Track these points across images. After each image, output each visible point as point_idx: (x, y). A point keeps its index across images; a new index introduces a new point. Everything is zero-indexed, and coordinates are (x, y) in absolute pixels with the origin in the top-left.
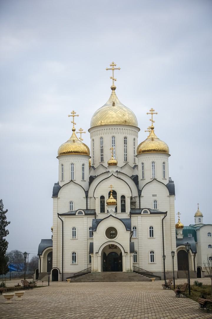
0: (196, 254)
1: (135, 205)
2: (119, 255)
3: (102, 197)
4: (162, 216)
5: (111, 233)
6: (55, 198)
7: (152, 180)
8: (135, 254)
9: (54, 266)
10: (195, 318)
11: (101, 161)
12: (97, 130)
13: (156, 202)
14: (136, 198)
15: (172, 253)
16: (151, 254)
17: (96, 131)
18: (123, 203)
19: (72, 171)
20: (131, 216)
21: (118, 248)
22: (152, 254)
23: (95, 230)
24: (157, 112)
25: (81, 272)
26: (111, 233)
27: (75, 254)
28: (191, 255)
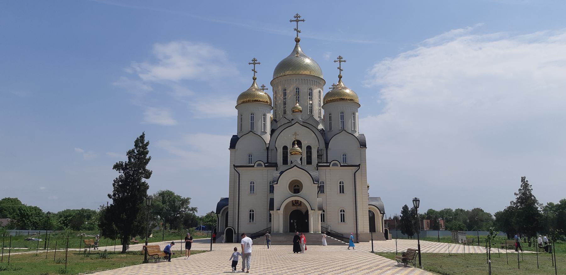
0: (384, 215)
1: (321, 159)
2: (304, 214)
3: (285, 148)
4: (356, 168)
5: (296, 187)
6: (232, 150)
7: (341, 131)
8: (323, 213)
9: (230, 224)
10: (351, 274)
11: (284, 114)
12: (280, 81)
13: (345, 156)
14: (323, 151)
15: (413, 201)
16: (341, 213)
17: (279, 82)
18: (309, 155)
19: (251, 121)
20: (318, 168)
21: (302, 205)
22: (342, 213)
23: (276, 183)
24: (343, 70)
25: (260, 232)
26: (296, 187)
27: (253, 211)
28: (379, 215)
